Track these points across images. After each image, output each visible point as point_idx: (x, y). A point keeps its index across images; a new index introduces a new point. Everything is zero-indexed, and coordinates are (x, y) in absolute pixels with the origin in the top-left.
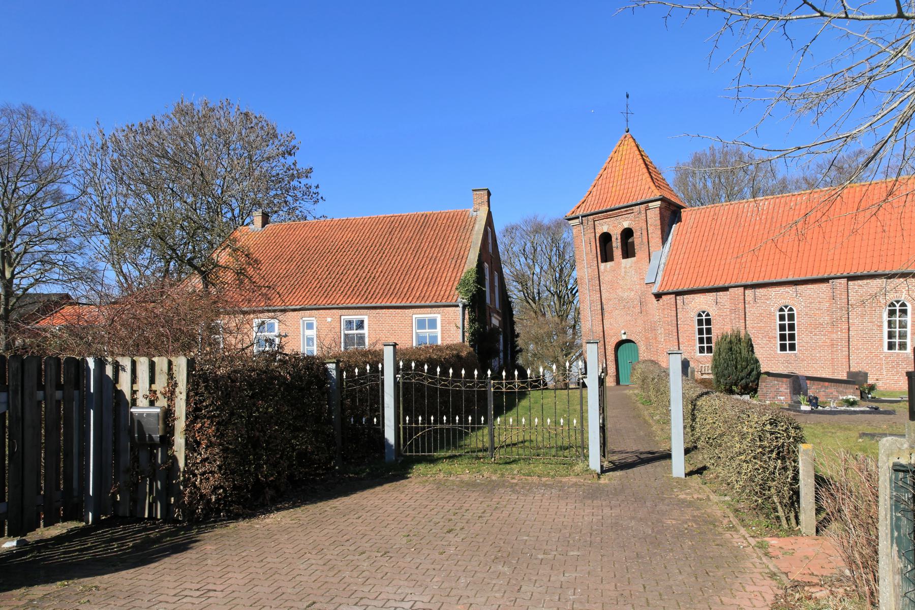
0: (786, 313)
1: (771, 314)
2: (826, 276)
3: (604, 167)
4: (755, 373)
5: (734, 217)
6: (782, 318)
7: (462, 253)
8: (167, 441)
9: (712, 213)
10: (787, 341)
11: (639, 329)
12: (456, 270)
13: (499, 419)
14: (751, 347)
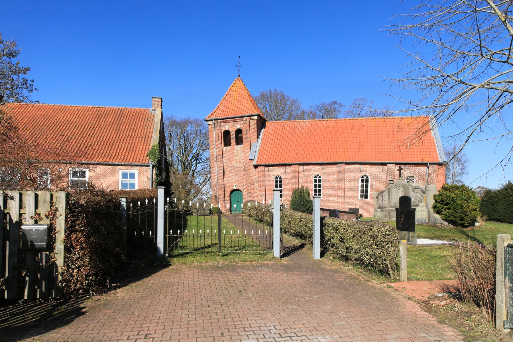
0: (318, 179)
1: (311, 179)
2: (336, 162)
3: (226, 94)
5: (293, 128)
6: (316, 181)
7: (148, 134)
8: (50, 247)
9: (282, 125)
12: (145, 144)
13: (186, 231)
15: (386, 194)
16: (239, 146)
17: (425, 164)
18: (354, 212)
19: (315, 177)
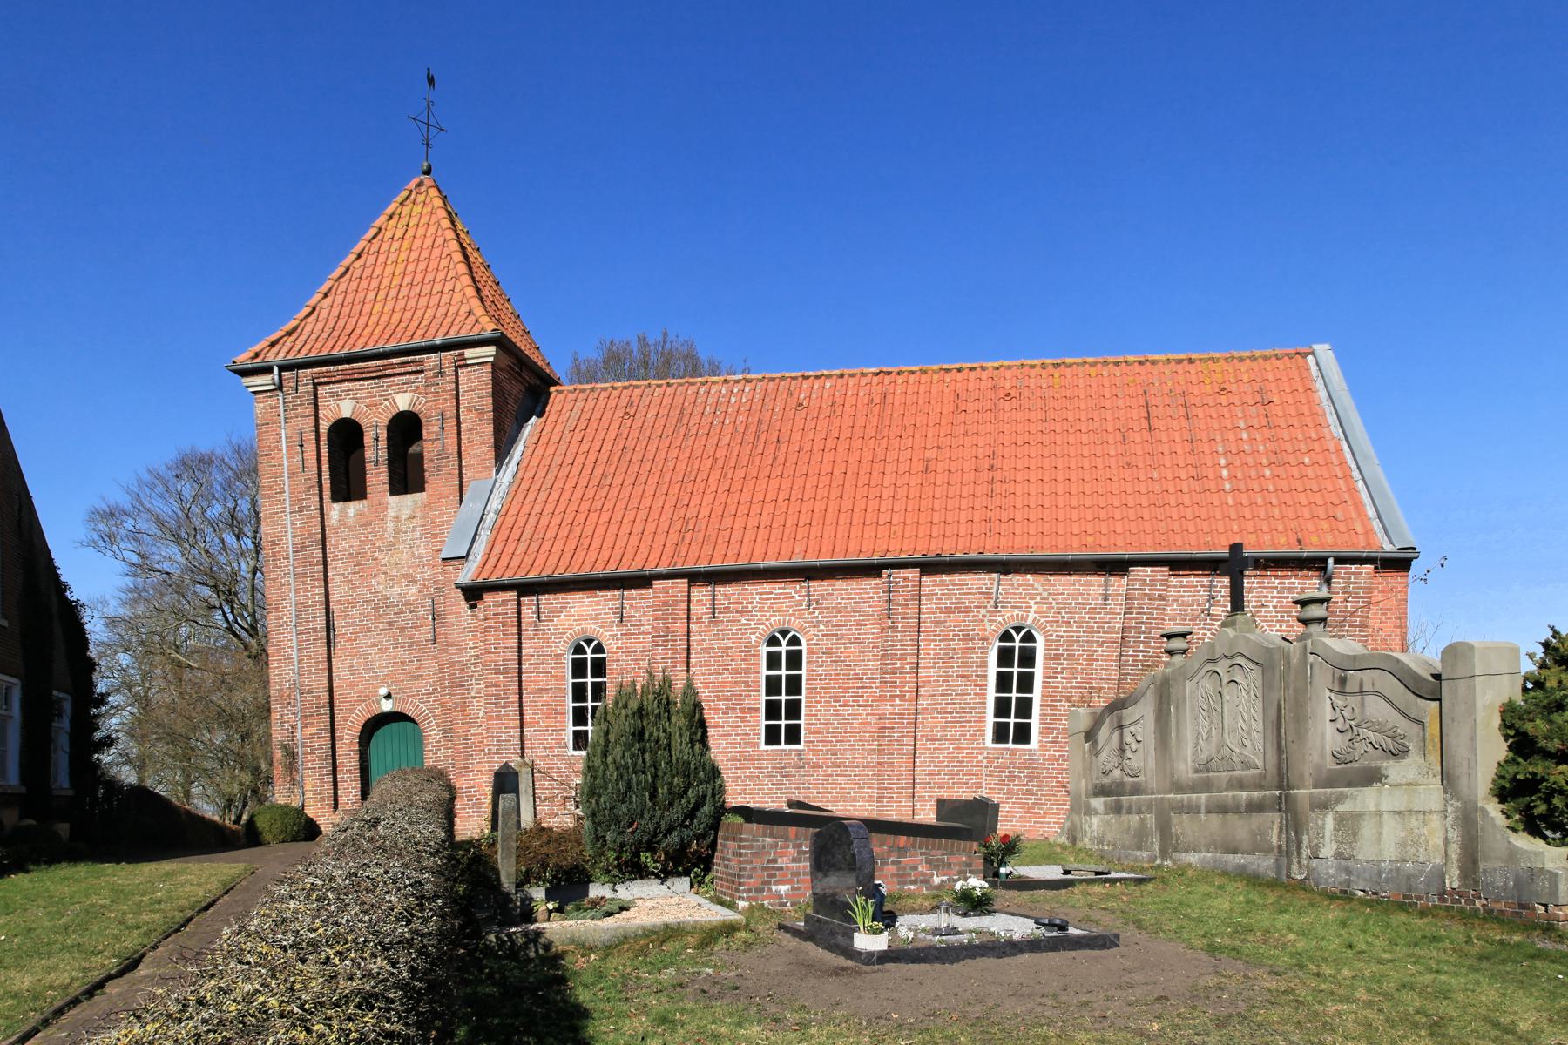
0: (784, 648)
1: (749, 651)
3: (357, 249)
4: (707, 809)
5: (675, 413)
6: (773, 661)
9: (624, 401)
10: (783, 720)
11: (427, 685)
14: (698, 727)
15: (1142, 717)
16: (410, 499)
17: (1316, 564)
18: (967, 823)
19: (773, 641)
